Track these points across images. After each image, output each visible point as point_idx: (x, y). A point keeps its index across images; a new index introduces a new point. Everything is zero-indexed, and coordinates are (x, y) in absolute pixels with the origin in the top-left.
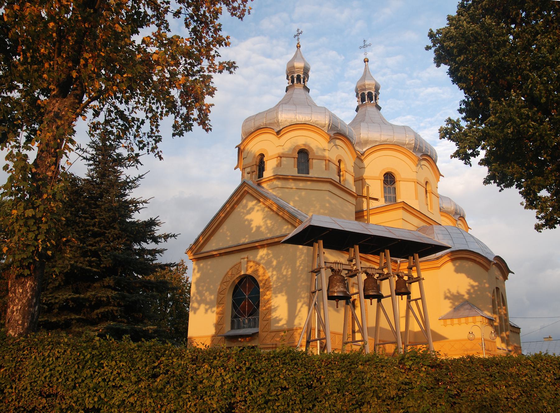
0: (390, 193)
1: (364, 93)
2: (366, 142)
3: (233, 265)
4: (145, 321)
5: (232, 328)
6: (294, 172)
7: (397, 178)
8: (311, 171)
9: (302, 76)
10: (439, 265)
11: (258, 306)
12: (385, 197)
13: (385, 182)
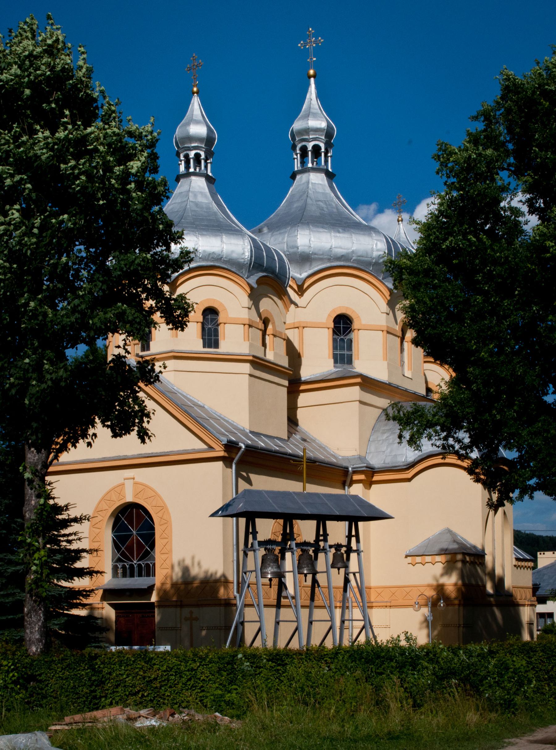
0: (342, 348)
2: (304, 259)
7: (355, 325)
8: (222, 343)
11: (152, 546)
13: (336, 331)
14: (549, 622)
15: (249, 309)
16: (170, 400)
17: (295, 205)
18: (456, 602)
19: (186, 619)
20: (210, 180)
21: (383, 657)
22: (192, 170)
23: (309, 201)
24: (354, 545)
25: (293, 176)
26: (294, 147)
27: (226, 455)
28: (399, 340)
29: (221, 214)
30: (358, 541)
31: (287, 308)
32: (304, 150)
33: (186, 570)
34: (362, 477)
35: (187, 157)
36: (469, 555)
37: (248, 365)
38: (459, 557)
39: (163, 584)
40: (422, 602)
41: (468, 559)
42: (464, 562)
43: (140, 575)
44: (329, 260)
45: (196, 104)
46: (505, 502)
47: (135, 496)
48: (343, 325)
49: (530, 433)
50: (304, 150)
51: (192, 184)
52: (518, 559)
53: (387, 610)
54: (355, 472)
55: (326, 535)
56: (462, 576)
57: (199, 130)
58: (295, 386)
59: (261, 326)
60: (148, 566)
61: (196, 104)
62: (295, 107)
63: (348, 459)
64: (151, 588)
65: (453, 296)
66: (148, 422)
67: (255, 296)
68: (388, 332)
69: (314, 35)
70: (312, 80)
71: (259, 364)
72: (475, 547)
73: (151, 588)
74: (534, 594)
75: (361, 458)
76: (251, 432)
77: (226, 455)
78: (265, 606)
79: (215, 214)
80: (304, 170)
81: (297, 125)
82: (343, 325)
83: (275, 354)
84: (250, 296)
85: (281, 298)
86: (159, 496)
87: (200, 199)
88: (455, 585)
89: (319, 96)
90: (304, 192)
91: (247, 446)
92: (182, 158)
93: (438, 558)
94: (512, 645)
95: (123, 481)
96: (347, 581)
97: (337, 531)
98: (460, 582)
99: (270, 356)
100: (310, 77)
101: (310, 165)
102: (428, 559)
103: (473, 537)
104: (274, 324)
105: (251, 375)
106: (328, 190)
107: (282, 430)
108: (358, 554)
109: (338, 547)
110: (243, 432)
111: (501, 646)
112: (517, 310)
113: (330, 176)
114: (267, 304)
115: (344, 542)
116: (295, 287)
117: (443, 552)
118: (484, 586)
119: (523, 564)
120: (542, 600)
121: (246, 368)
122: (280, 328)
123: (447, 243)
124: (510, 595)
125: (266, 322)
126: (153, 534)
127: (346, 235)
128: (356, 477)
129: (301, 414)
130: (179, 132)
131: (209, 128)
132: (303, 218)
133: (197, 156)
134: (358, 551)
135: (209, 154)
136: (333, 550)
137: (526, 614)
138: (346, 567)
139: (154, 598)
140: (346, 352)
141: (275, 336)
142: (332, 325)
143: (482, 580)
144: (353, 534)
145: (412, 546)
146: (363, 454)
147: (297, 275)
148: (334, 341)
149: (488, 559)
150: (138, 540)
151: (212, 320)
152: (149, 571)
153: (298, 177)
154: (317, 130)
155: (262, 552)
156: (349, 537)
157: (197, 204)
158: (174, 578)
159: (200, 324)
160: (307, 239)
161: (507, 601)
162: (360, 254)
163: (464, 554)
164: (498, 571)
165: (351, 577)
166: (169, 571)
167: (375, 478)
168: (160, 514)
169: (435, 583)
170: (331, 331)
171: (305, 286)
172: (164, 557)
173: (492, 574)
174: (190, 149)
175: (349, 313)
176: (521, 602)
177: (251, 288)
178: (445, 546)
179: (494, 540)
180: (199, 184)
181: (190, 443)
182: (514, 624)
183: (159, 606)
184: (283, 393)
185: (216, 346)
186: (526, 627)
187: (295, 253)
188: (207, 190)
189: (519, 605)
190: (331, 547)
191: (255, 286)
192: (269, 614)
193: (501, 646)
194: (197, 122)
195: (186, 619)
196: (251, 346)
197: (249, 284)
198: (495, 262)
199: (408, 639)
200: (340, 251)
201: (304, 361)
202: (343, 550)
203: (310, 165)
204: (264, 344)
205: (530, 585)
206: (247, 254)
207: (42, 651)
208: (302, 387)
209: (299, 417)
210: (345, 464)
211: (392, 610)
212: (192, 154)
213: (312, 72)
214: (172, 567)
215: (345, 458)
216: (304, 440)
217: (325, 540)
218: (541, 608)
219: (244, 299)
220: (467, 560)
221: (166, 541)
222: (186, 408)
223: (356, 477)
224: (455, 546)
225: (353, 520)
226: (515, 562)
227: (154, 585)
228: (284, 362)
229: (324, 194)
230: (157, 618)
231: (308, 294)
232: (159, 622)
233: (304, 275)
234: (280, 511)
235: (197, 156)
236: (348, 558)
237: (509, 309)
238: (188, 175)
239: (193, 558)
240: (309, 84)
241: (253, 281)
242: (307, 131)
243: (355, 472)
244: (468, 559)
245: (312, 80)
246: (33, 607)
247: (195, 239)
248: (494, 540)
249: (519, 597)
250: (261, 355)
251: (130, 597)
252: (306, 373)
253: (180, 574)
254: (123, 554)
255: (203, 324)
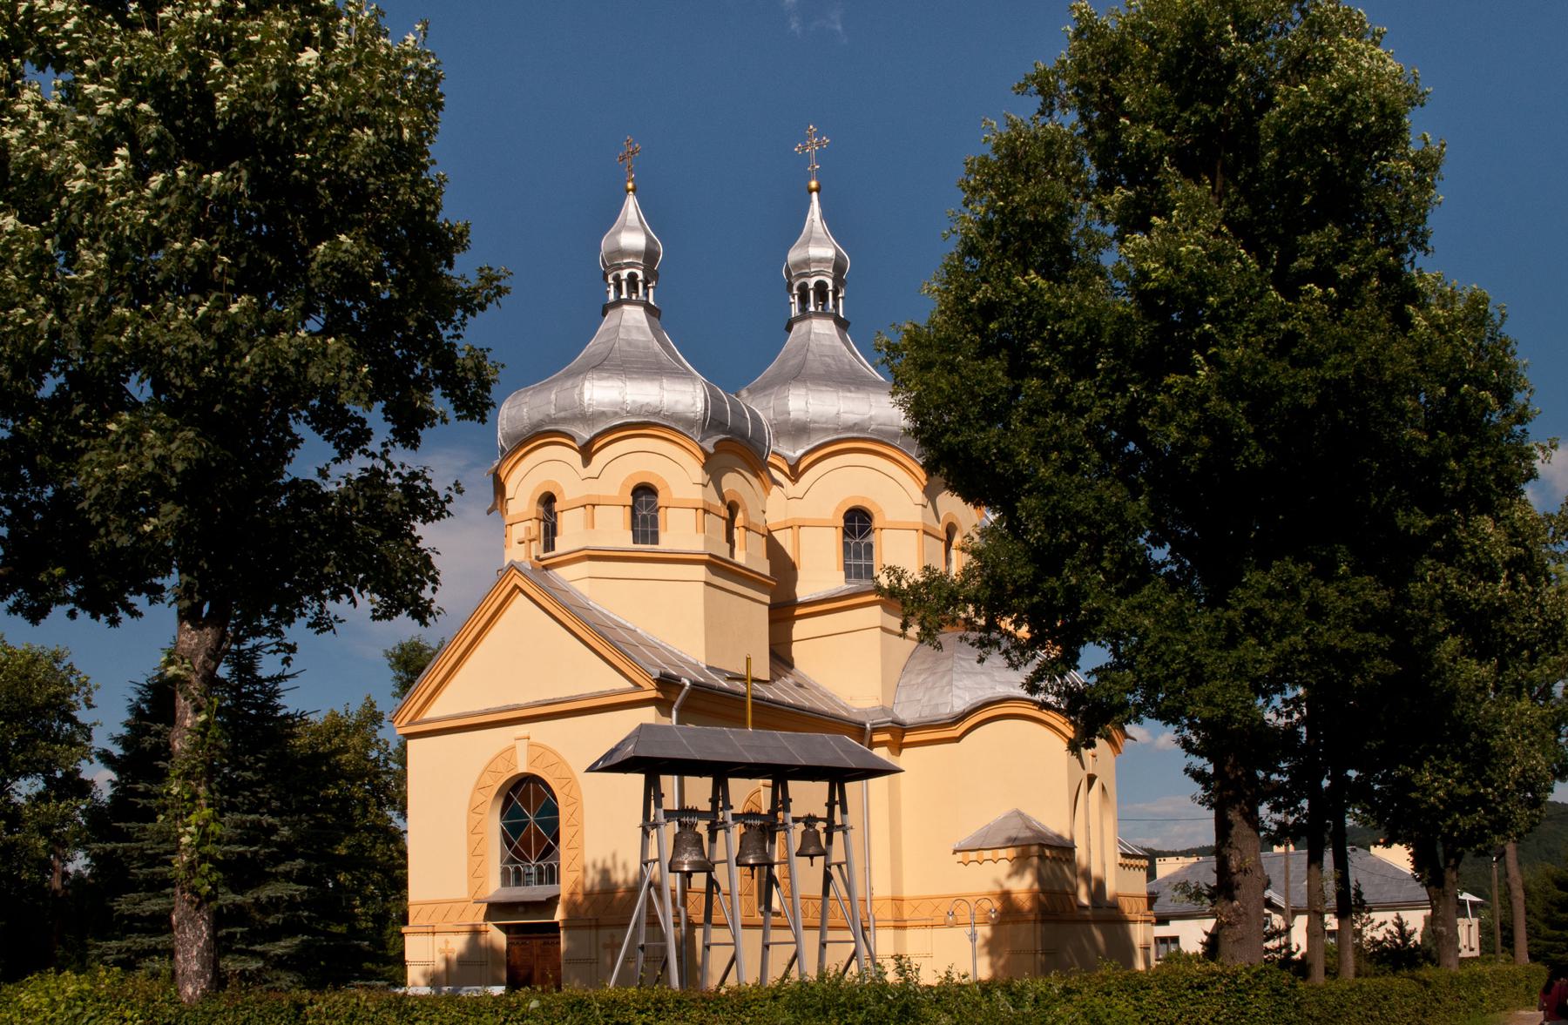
0: (858, 556)
1: (805, 285)
2: (800, 430)
3: (497, 751)
4: (1093, 680)
5: (505, 881)
6: (623, 539)
7: (876, 523)
8: (662, 536)
9: (640, 275)
10: (957, 733)
11: (556, 839)
12: (847, 568)
13: (848, 531)
14: (1173, 948)
15: (705, 486)
16: (578, 618)
17: (791, 363)
18: (1032, 917)
19: (606, 946)
20: (649, 310)
21: (844, 1005)
22: (624, 296)
23: (810, 356)
24: (838, 820)
25: (789, 328)
26: (790, 286)
27: (660, 695)
28: (942, 545)
29: (664, 356)
30: (844, 811)
31: (767, 490)
32: (803, 290)
33: (605, 873)
34: (886, 737)
35: (617, 279)
36: (1050, 847)
37: (702, 568)
38: (1034, 849)
39: (572, 894)
40: (979, 918)
41: (1048, 853)
42: (1042, 857)
43: (540, 882)
44: (836, 430)
45: (631, 205)
46: (1097, 740)
47: (531, 763)
48: (858, 522)
49: (1131, 609)
50: (803, 290)
51: (625, 316)
52: (1124, 855)
53: (928, 931)
54: (875, 730)
55: (787, 801)
56: (1040, 878)
57: (633, 240)
58: (784, 611)
59: (725, 512)
60: (551, 866)
61: (631, 205)
62: (793, 229)
63: (865, 712)
64: (552, 902)
65: (990, 380)
66: (434, 590)
67: (714, 467)
68: (925, 532)
69: (816, 134)
70: (815, 195)
71: (717, 566)
72: (1060, 837)
73: (552, 902)
74: (1150, 908)
75: (884, 710)
76: (708, 668)
77: (660, 695)
78: (744, 926)
79: (656, 355)
80: (805, 314)
81: (794, 256)
82: (858, 522)
83: (749, 554)
84: (706, 467)
85: (757, 476)
86: (565, 762)
87: (636, 337)
88: (1030, 890)
89: (825, 216)
90: (805, 347)
91: (695, 684)
92: (610, 281)
93: (1002, 853)
94: (1105, 978)
95: (512, 742)
96: (828, 878)
97: (808, 797)
98: (1036, 887)
99: (740, 558)
100: (811, 191)
101: (812, 309)
102: (987, 854)
103: (1055, 822)
104: (745, 511)
105: (707, 583)
106: (838, 342)
107: (762, 669)
108: (845, 832)
109: (810, 820)
110: (695, 667)
111: (1086, 979)
112: (1102, 396)
113: (842, 324)
114: (733, 482)
115: (822, 812)
116: (787, 470)
117: (1012, 842)
118: (1075, 894)
119: (1133, 862)
120: (1163, 920)
121: (701, 572)
122: (755, 519)
123: (979, 294)
124: (1114, 906)
125: (733, 508)
126: (557, 822)
127: (860, 395)
128: (876, 738)
129: (797, 651)
130: (606, 245)
131: (648, 236)
132: (800, 375)
133: (632, 277)
134: (844, 828)
135: (651, 275)
136: (801, 827)
137: (1141, 934)
138: (825, 853)
139: (559, 915)
140: (863, 562)
141: (747, 529)
142: (842, 523)
143: (1071, 885)
144: (837, 801)
145: (963, 836)
146: (888, 705)
147: (789, 453)
148: (846, 545)
149: (1080, 853)
150: (537, 833)
151: (648, 504)
152: (551, 875)
153: (796, 327)
154: (820, 261)
155: (673, 828)
156: (831, 805)
157: (629, 343)
158: (588, 884)
159: (628, 510)
160: (803, 403)
161: (1110, 915)
162: (881, 420)
163: (1042, 846)
164: (1095, 871)
165: (834, 871)
166: (580, 874)
167: (907, 739)
168: (566, 790)
169: (998, 890)
170: (840, 531)
171: (801, 467)
172: (572, 853)
173: (1086, 875)
174: (620, 267)
175: (866, 505)
176: (1131, 917)
177: (707, 455)
178: (1013, 834)
179: (1088, 827)
180: (634, 315)
181: (604, 680)
182: (1124, 950)
183: (566, 928)
184: (759, 616)
185: (655, 541)
186: (1139, 953)
187: (786, 422)
188: (646, 324)
189: (1128, 921)
190: (796, 820)
191: (711, 450)
192: (751, 942)
193: (1086, 979)
194: (632, 229)
195: (606, 946)
196: (707, 541)
197: (702, 449)
198: (1061, 315)
199: (901, 969)
200: (852, 418)
201: (801, 574)
202: (820, 826)
203: (812, 309)
204: (730, 539)
205: (1144, 892)
206: (700, 406)
207: (204, 994)
208: (798, 612)
209: (794, 654)
210: (860, 719)
211: (935, 931)
212: (624, 274)
213: (813, 184)
214: (585, 870)
215: (861, 712)
216: (800, 686)
217: (787, 809)
218: (1162, 931)
219: (696, 472)
220: (1049, 855)
221: (574, 829)
222: (604, 630)
223: (876, 738)
224: (1029, 834)
225: (837, 777)
226: (1120, 860)
227: (558, 897)
228: (763, 567)
229: (833, 347)
230: (563, 946)
231: (806, 479)
232: (567, 951)
233: (799, 452)
234: (698, 757)
235: (632, 277)
236: (829, 841)
237: (1088, 396)
238: (619, 303)
239: (614, 856)
240: (810, 201)
241: (709, 445)
242: (807, 262)
243: (875, 730)
244: (1048, 853)
245: (815, 195)
246: (187, 913)
247: (620, 384)
248: (1088, 827)
249: (1127, 911)
250: (725, 554)
251: (525, 915)
252: (803, 592)
253: (597, 878)
254: (516, 852)
255: (633, 509)
